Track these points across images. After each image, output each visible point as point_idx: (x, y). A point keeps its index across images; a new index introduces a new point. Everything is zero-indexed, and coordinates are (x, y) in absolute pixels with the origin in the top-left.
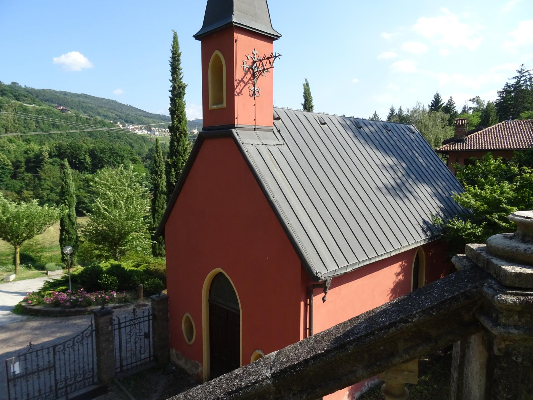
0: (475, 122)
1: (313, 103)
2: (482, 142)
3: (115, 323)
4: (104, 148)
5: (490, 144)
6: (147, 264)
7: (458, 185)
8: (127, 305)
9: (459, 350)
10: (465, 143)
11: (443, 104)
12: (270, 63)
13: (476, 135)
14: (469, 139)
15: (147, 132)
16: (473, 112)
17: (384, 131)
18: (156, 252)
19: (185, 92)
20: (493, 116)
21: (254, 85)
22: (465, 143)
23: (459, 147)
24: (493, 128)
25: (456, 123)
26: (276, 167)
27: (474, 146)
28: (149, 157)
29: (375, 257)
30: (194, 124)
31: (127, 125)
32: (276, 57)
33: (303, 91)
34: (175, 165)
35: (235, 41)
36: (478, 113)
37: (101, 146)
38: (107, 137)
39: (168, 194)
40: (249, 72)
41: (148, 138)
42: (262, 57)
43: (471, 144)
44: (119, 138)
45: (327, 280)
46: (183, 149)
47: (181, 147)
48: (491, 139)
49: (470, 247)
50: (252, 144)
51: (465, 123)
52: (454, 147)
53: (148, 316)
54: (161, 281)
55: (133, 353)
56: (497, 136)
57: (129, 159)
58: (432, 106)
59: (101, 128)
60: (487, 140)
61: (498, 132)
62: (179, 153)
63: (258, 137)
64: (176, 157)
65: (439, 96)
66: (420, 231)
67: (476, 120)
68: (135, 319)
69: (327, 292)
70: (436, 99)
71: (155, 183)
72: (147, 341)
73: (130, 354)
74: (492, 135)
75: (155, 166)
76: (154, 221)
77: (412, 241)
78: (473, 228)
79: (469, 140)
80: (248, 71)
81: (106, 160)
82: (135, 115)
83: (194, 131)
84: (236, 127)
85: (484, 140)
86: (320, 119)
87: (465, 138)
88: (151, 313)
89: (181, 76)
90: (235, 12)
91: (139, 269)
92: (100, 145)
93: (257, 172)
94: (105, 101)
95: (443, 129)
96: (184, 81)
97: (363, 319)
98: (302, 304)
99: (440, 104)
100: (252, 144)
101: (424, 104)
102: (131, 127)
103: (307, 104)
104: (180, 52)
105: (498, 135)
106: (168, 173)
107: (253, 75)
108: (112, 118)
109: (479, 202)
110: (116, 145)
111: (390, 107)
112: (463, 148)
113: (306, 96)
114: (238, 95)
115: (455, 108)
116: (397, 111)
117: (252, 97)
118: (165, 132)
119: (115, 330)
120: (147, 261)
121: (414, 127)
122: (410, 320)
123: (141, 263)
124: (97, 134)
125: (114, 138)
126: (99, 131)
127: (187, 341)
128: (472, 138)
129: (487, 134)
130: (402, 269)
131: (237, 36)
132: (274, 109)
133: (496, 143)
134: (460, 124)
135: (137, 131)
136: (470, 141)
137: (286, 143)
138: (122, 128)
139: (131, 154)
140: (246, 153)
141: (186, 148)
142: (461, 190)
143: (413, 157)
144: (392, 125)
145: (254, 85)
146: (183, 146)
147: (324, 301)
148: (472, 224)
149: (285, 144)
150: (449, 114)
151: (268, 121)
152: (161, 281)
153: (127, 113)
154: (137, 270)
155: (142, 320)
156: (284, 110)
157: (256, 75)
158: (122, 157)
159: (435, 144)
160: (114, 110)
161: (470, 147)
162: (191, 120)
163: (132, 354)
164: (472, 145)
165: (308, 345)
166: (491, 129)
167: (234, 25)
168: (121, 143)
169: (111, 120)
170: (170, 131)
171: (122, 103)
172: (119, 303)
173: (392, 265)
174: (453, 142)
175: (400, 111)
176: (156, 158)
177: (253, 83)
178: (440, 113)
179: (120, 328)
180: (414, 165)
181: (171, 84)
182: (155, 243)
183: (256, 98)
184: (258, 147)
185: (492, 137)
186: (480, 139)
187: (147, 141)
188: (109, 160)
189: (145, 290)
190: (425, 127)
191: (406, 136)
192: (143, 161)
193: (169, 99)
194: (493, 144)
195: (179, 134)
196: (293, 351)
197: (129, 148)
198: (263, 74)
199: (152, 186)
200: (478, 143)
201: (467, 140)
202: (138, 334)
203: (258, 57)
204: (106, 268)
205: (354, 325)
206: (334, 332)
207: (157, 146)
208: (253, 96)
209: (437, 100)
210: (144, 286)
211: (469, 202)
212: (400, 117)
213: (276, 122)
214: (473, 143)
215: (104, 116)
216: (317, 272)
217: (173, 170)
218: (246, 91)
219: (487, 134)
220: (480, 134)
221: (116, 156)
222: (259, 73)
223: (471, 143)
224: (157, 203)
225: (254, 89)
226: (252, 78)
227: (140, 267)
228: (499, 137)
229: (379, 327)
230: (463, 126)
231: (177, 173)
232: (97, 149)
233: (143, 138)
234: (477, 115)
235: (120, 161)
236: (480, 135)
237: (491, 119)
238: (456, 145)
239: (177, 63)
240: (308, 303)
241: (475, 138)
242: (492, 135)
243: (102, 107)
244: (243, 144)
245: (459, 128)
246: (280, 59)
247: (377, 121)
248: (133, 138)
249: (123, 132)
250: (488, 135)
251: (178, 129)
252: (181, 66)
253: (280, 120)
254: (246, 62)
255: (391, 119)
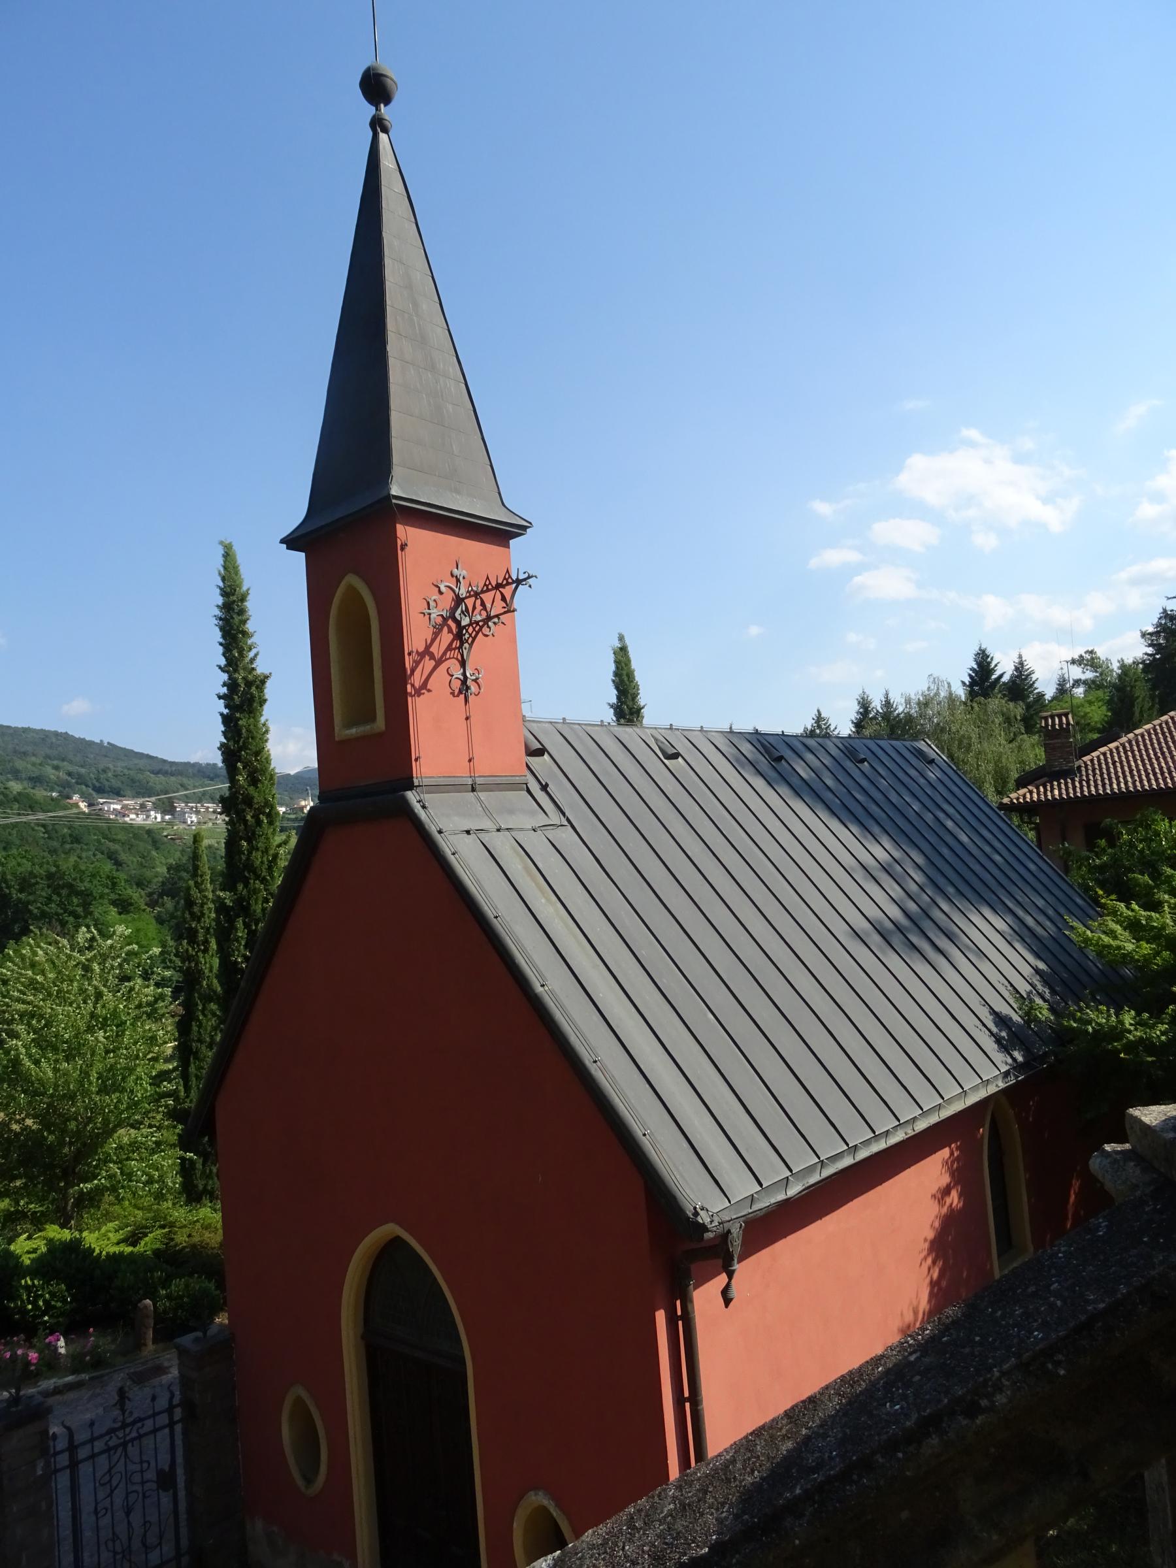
0: (1096, 719)
1: (642, 700)
2: (1124, 772)
3: (58, 1448)
4: (31, 873)
5: (1147, 775)
6: (167, 1230)
7: (1079, 901)
8: (102, 1376)
9: (1165, 1478)
10: (1077, 779)
11: (1001, 676)
12: (503, 599)
13: (1104, 754)
14: (1086, 766)
15: (162, 818)
16: (1085, 692)
17: (848, 765)
18: (196, 1186)
19: (267, 697)
20: (1140, 699)
21: (463, 663)
22: (1077, 779)
23: (1064, 792)
24: (1146, 731)
25: (1043, 724)
26: (543, 893)
27: (1104, 785)
28: (170, 889)
29: (867, 1143)
30: (295, 784)
31: (101, 801)
32: (519, 582)
33: (612, 667)
34: (242, 907)
35: (402, 545)
36: (1100, 693)
37: (20, 870)
38: (42, 842)
39: (224, 1002)
40: (446, 629)
41: (165, 834)
42: (481, 584)
43: (1095, 781)
44: (76, 839)
45: (729, 1232)
46: (265, 859)
47: (260, 853)
48: (1147, 762)
49: (1140, 1121)
50: (468, 832)
51: (1068, 723)
52: (1049, 794)
53: (170, 1410)
54: (210, 1281)
55: (118, 1549)
56: (1163, 753)
57: (106, 901)
58: (973, 682)
59: (24, 815)
60: (1137, 766)
61: (1162, 740)
62: (255, 873)
63: (485, 809)
64: (246, 884)
65: (988, 657)
66: (990, 1045)
67: (1098, 714)
68: (124, 1426)
69: (733, 1271)
70: (979, 664)
71: (189, 968)
72: (166, 1499)
73: (111, 1554)
74: (1147, 750)
75: (187, 915)
76: (187, 1088)
77: (971, 1082)
78: (1139, 1023)
79: (1087, 770)
80: (442, 626)
81: (36, 911)
82: (126, 771)
83: (303, 803)
84: (416, 783)
85: (1130, 766)
86: (662, 742)
87: (1077, 764)
88: (176, 1401)
89: (251, 654)
90: (397, 471)
91: (140, 1248)
92: (19, 865)
93: (490, 913)
94: (35, 735)
95: (1011, 745)
96: (261, 667)
97: (831, 1406)
98: (661, 1317)
99: (994, 677)
100: (468, 832)
101: (949, 680)
102: (113, 806)
103: (625, 703)
104: (244, 588)
105: (1165, 750)
106: (225, 935)
107: (459, 636)
108: (56, 784)
109: (1147, 943)
110: (68, 863)
111: (856, 694)
112: (1075, 792)
113: (622, 681)
114: (418, 693)
115: (1035, 685)
116: (877, 704)
117: (458, 696)
118: (214, 812)
119: (58, 1474)
120: (165, 1219)
121: (930, 746)
122: (985, 1401)
123: (147, 1228)
124: (10, 834)
125: (64, 843)
126: (15, 825)
127: (300, 1482)
128: (1096, 762)
129: (1135, 748)
130: (952, 1175)
131: (404, 532)
132: (526, 724)
133: (1162, 773)
134: (1057, 727)
135: (133, 816)
136: (1090, 772)
137: (568, 820)
138: (86, 810)
139: (114, 884)
140: (452, 859)
141: (276, 856)
142: (1093, 909)
143: (942, 832)
144: (870, 746)
145: (463, 663)
146: (266, 851)
147: (727, 1301)
148: (1138, 1014)
149: (566, 823)
150: (1021, 703)
151: (511, 762)
152: (210, 1281)
153: (101, 766)
154: (132, 1252)
155: (149, 1425)
156: (556, 725)
157: (467, 636)
158: (88, 895)
159: (995, 787)
160: (63, 760)
161: (1093, 789)
162: (292, 773)
163: (115, 1553)
164: (1099, 782)
165: (657, 1524)
166: (1142, 736)
167: (396, 504)
168: (84, 855)
169: (52, 790)
170: (226, 810)
171: (87, 739)
172: (73, 1374)
173: (922, 1159)
174: (1045, 779)
175: (888, 704)
176: (192, 892)
177: (459, 657)
178: (996, 703)
179: (74, 1465)
180: (945, 851)
181: (225, 677)
182: (191, 1160)
183: (471, 698)
184: (485, 837)
185: (1148, 755)
186: (1118, 764)
187: (163, 844)
188: (45, 908)
189: (159, 1317)
190: (960, 742)
191: (913, 772)
192: (152, 904)
193: (220, 719)
194: (1155, 774)
195: (252, 817)
196: (605, 1552)
197: (108, 867)
198: (485, 630)
199: (177, 977)
200: (1113, 775)
201: (1083, 769)
202: (137, 1478)
203: (470, 585)
204: (33, 1256)
205: (804, 1431)
206: (739, 1465)
207: (195, 857)
208: (460, 692)
209: (983, 667)
210: (155, 1305)
211: (1119, 948)
212: (888, 721)
213: (534, 761)
214: (1099, 778)
215: (30, 779)
216: (695, 1208)
217: (239, 923)
218: (439, 681)
219: (1135, 748)
220: (1114, 751)
221: (69, 895)
222: (474, 629)
223: (1094, 776)
224: (195, 1028)
225: (464, 674)
226: (456, 644)
227: (143, 1243)
228: (1167, 754)
229: (885, 1437)
230: (1064, 731)
231: (251, 934)
232: (9, 877)
233: (151, 835)
234: (1098, 700)
235: (80, 910)
236: (1115, 754)
237: (1137, 710)
238: (1056, 787)
239: (237, 619)
240: (679, 1313)
241: (1103, 761)
242: (1147, 750)
243: (25, 753)
244: (440, 832)
245: (1054, 739)
246: (530, 586)
247: (827, 736)
248: (119, 837)
249: (88, 822)
250: (1137, 753)
251: (248, 801)
252: (250, 626)
253: (546, 756)
254: (435, 601)
255: (863, 727)
